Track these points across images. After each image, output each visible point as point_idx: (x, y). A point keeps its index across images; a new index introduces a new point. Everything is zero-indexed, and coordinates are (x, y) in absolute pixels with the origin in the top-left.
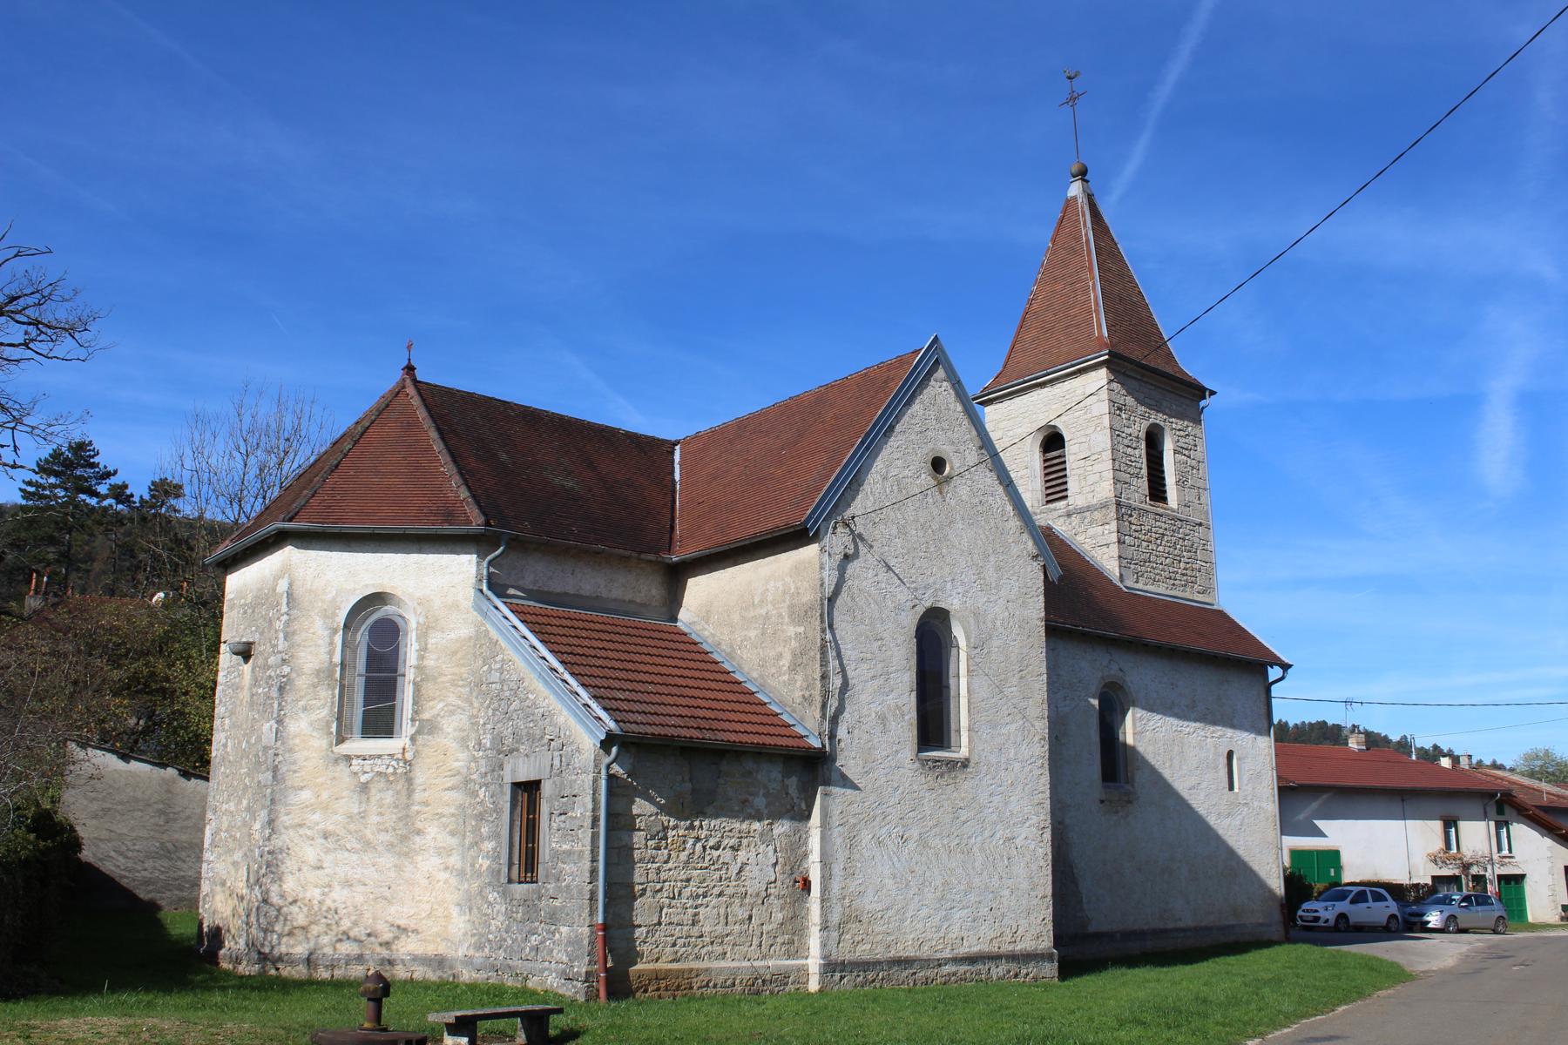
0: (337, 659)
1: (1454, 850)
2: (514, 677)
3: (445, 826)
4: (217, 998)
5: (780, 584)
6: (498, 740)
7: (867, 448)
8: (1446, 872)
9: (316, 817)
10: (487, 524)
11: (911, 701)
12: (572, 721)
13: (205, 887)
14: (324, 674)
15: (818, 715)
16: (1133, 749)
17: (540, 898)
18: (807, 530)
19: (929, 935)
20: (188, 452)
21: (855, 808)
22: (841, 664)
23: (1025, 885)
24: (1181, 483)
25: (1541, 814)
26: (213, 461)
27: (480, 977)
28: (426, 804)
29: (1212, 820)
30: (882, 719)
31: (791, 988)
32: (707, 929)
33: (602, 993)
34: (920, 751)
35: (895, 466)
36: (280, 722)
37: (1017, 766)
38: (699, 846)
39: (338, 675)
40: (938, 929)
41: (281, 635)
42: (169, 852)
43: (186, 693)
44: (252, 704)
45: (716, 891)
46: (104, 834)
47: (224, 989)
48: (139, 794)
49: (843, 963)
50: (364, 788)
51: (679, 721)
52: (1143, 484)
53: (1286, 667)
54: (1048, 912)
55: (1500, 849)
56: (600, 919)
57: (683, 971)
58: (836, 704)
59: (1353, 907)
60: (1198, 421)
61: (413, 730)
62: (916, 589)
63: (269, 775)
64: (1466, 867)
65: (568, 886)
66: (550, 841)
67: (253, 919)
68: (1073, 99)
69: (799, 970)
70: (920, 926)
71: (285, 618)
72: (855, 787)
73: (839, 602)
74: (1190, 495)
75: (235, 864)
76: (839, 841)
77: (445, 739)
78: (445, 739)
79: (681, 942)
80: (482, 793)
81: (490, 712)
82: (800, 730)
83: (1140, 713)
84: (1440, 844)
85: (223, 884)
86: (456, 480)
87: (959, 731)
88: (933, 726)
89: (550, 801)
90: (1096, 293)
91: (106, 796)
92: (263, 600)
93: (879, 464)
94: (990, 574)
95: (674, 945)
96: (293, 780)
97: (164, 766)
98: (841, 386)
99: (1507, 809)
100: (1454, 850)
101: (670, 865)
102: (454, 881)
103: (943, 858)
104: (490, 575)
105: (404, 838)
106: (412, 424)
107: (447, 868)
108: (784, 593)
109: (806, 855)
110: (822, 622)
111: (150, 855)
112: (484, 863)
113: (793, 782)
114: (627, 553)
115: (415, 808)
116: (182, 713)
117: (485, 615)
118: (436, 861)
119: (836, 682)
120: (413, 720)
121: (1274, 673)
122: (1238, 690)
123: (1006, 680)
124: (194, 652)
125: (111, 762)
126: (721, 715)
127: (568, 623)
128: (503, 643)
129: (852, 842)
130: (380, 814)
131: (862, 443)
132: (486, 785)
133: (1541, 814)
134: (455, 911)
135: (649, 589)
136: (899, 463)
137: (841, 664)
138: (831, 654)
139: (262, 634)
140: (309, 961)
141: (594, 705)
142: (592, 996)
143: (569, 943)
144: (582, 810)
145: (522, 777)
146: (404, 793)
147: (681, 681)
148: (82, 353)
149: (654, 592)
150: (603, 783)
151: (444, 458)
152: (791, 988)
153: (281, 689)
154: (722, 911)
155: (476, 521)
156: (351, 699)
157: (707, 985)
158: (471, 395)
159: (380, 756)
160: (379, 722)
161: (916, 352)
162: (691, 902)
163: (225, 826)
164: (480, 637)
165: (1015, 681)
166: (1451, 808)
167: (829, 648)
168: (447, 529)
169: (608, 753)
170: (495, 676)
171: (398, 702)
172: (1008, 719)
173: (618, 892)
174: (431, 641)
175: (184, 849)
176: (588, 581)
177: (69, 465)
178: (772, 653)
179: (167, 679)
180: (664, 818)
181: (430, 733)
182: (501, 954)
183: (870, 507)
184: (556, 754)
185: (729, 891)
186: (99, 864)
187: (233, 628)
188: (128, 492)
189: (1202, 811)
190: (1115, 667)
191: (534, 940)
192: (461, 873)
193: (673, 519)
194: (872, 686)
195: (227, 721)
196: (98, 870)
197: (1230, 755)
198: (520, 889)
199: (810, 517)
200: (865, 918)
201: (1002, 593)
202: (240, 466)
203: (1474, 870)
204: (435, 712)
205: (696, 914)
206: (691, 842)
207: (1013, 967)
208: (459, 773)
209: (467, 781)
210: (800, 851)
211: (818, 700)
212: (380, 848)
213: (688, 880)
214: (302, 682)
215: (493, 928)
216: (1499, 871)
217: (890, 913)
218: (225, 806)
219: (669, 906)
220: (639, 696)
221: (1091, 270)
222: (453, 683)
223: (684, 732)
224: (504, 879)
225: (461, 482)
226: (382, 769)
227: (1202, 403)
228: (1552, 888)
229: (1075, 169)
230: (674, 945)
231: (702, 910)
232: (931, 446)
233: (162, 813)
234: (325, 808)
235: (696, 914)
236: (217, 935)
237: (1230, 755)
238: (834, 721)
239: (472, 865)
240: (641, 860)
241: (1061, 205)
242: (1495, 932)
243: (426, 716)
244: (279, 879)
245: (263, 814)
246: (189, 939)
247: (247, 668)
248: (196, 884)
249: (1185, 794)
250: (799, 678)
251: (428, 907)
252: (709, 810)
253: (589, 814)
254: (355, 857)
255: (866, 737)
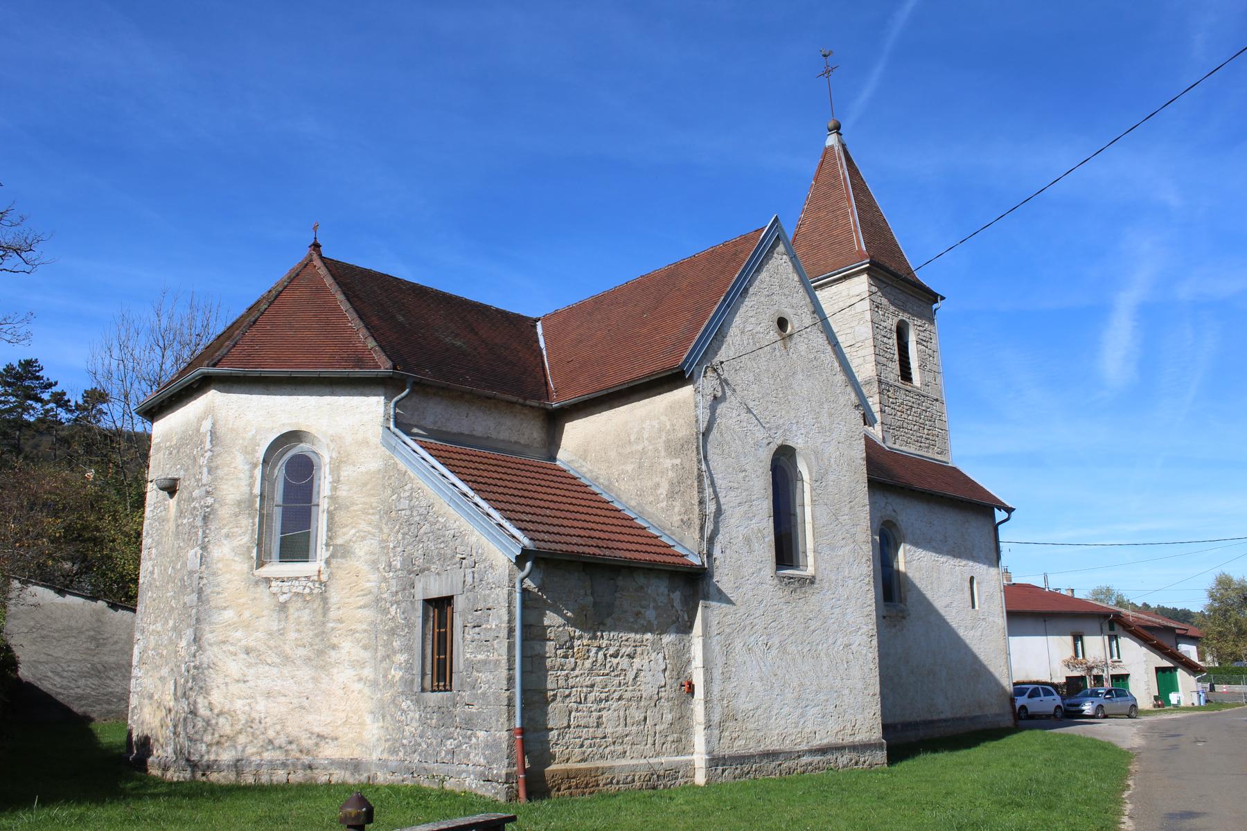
0: (257, 490)
1: (1081, 657)
2: (424, 503)
3: (358, 641)
4: (150, 808)
5: (655, 423)
6: (409, 561)
7: (728, 306)
8: (1076, 673)
9: (239, 634)
10: (394, 368)
11: (769, 525)
12: (484, 540)
13: (134, 701)
14: (244, 505)
15: (697, 535)
16: (905, 574)
17: (455, 705)
18: (683, 372)
19: (790, 730)
20: (116, 343)
21: (729, 619)
22: (715, 491)
23: (860, 685)
24: (922, 367)
25: (1140, 630)
26: (136, 353)
27: (398, 778)
28: (340, 621)
29: (961, 632)
30: (748, 540)
31: (681, 781)
32: (609, 730)
33: (522, 793)
34: (778, 569)
35: (749, 323)
36: (204, 548)
37: (851, 582)
38: (601, 654)
39: (258, 505)
40: (797, 724)
41: (205, 470)
42: (99, 672)
43: (114, 541)
44: (177, 534)
45: (616, 695)
46: (43, 658)
47: (154, 796)
48: (73, 623)
49: (724, 757)
50: (283, 607)
51: (579, 541)
52: (896, 367)
53: (1009, 510)
54: (877, 708)
55: (1112, 656)
56: (518, 723)
57: (590, 770)
58: (712, 527)
59: (1031, 700)
60: (932, 321)
61: (327, 555)
62: (770, 429)
63: (194, 596)
64: (1090, 669)
65: (484, 694)
66: (464, 651)
67: (180, 729)
68: (828, 72)
69: (687, 765)
70: (783, 722)
71: (208, 454)
72: (729, 601)
73: (711, 437)
74: (929, 378)
75: (162, 679)
76: (717, 648)
77: (358, 563)
78: (358, 563)
79: (587, 743)
80: (393, 610)
81: (400, 536)
82: (679, 550)
83: (908, 547)
84: (1071, 653)
85: (151, 697)
86: (363, 333)
87: (805, 552)
88: (786, 551)
89: (463, 614)
90: (854, 218)
91: (46, 628)
92: (189, 439)
93: (738, 320)
94: (824, 419)
95: (582, 746)
96: (216, 601)
97: (94, 598)
98: (692, 262)
99: (1116, 626)
100: (1081, 657)
101: (577, 672)
102: (367, 691)
103: (788, 668)
104: (396, 415)
105: (320, 653)
106: (321, 289)
107: (360, 680)
108: (660, 430)
109: (689, 662)
110: (698, 453)
111: (83, 675)
112: (397, 674)
113: (677, 596)
114: (514, 399)
115: (331, 625)
116: (110, 558)
117: (393, 449)
118: (351, 673)
119: (711, 508)
120: (327, 545)
121: (1000, 515)
122: (974, 527)
123: (840, 508)
124: (120, 507)
125: (45, 595)
126: (612, 536)
127: (468, 458)
128: (411, 473)
129: (728, 650)
130: (298, 631)
131: (724, 300)
132: (398, 603)
133: (1140, 630)
134: (368, 719)
135: (530, 432)
136: (753, 320)
137: (715, 491)
138: (707, 482)
139: (186, 470)
140: (237, 766)
141: (506, 524)
142: (512, 797)
143: (487, 746)
144: (498, 621)
145: (434, 594)
146: (320, 611)
147: (571, 508)
148: (28, 268)
149: (535, 435)
150: (518, 596)
151: (351, 315)
152: (681, 781)
153: (205, 518)
154: (622, 713)
155: (384, 366)
156: (270, 527)
157: (611, 783)
158: (369, 271)
159: (297, 578)
160: (295, 547)
161: (763, 229)
162: (595, 706)
163: (152, 644)
164: (389, 470)
165: (846, 510)
166: (1078, 626)
167: (704, 478)
168: (358, 372)
169: (522, 568)
170: (405, 504)
171: (312, 530)
172: (843, 543)
173: (534, 698)
174: (343, 474)
175: (112, 669)
176: (481, 423)
177: (19, 377)
178: (650, 484)
179: (97, 529)
180: (571, 629)
181: (344, 556)
182: (416, 757)
183: (732, 354)
184: (469, 571)
185: (627, 695)
186: (37, 684)
187: (158, 468)
188: (66, 398)
189: (954, 625)
190: (890, 508)
191: (450, 744)
192: (374, 684)
193: (545, 376)
194: (739, 511)
195: (154, 551)
196: (37, 688)
197: (972, 579)
198: (434, 698)
199: (686, 362)
200: (739, 717)
201: (834, 436)
202: (159, 358)
203: (1095, 672)
204: (347, 537)
205: (600, 717)
206: (594, 650)
207: (854, 755)
208: (370, 593)
209: (378, 600)
210: (685, 658)
211: (697, 522)
212: (298, 662)
213: (592, 686)
214: (224, 512)
215: (407, 733)
216: (1111, 672)
217: (760, 711)
218: (152, 632)
219: (577, 710)
220: (539, 519)
221: (849, 200)
222: (364, 512)
223: (587, 550)
224: (417, 688)
225: (368, 334)
226: (300, 590)
227: (935, 306)
228: (1147, 683)
229: (831, 125)
230: (582, 746)
231: (604, 713)
232: (776, 307)
233: (93, 638)
234: (247, 626)
235: (600, 717)
236: (145, 745)
237: (972, 579)
238: (711, 541)
239: (385, 676)
240: (552, 668)
241: (822, 152)
242: (1130, 717)
243: (339, 541)
244: (204, 690)
245: (189, 633)
246: (120, 747)
247: (172, 502)
248: (124, 697)
249: (942, 611)
250: (678, 505)
251: (343, 715)
252: (609, 621)
253: (505, 625)
254: (275, 670)
255: (735, 556)
